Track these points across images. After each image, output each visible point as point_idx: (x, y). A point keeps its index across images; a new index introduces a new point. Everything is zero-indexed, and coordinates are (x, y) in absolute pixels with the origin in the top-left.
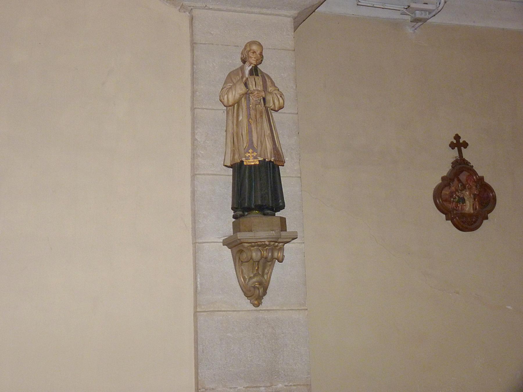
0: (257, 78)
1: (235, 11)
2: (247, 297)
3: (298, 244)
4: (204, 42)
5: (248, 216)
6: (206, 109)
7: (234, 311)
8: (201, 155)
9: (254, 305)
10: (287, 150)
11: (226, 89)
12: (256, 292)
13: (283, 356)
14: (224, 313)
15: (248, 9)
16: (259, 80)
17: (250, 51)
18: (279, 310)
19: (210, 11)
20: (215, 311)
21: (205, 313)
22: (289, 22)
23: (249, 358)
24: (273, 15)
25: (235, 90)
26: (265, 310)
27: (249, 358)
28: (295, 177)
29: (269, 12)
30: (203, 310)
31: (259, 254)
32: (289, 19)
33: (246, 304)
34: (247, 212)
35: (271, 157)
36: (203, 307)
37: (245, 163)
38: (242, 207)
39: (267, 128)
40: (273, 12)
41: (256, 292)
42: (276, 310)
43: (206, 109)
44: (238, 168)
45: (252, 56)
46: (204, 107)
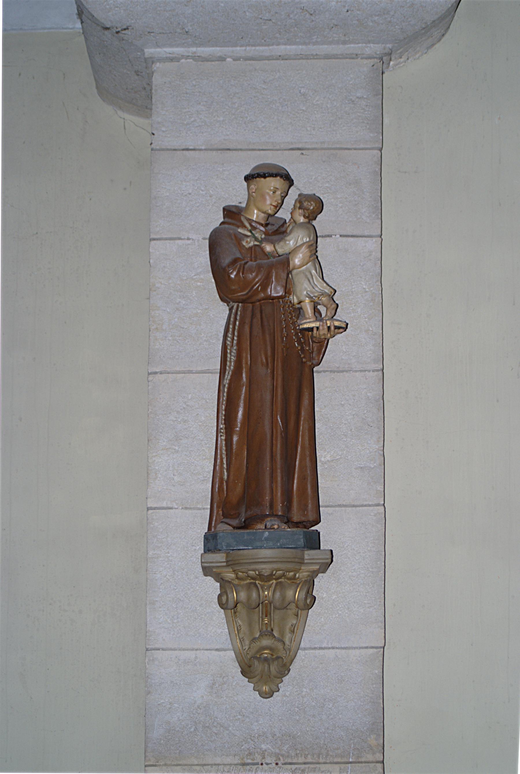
31: (254, 595)
33: (245, 691)
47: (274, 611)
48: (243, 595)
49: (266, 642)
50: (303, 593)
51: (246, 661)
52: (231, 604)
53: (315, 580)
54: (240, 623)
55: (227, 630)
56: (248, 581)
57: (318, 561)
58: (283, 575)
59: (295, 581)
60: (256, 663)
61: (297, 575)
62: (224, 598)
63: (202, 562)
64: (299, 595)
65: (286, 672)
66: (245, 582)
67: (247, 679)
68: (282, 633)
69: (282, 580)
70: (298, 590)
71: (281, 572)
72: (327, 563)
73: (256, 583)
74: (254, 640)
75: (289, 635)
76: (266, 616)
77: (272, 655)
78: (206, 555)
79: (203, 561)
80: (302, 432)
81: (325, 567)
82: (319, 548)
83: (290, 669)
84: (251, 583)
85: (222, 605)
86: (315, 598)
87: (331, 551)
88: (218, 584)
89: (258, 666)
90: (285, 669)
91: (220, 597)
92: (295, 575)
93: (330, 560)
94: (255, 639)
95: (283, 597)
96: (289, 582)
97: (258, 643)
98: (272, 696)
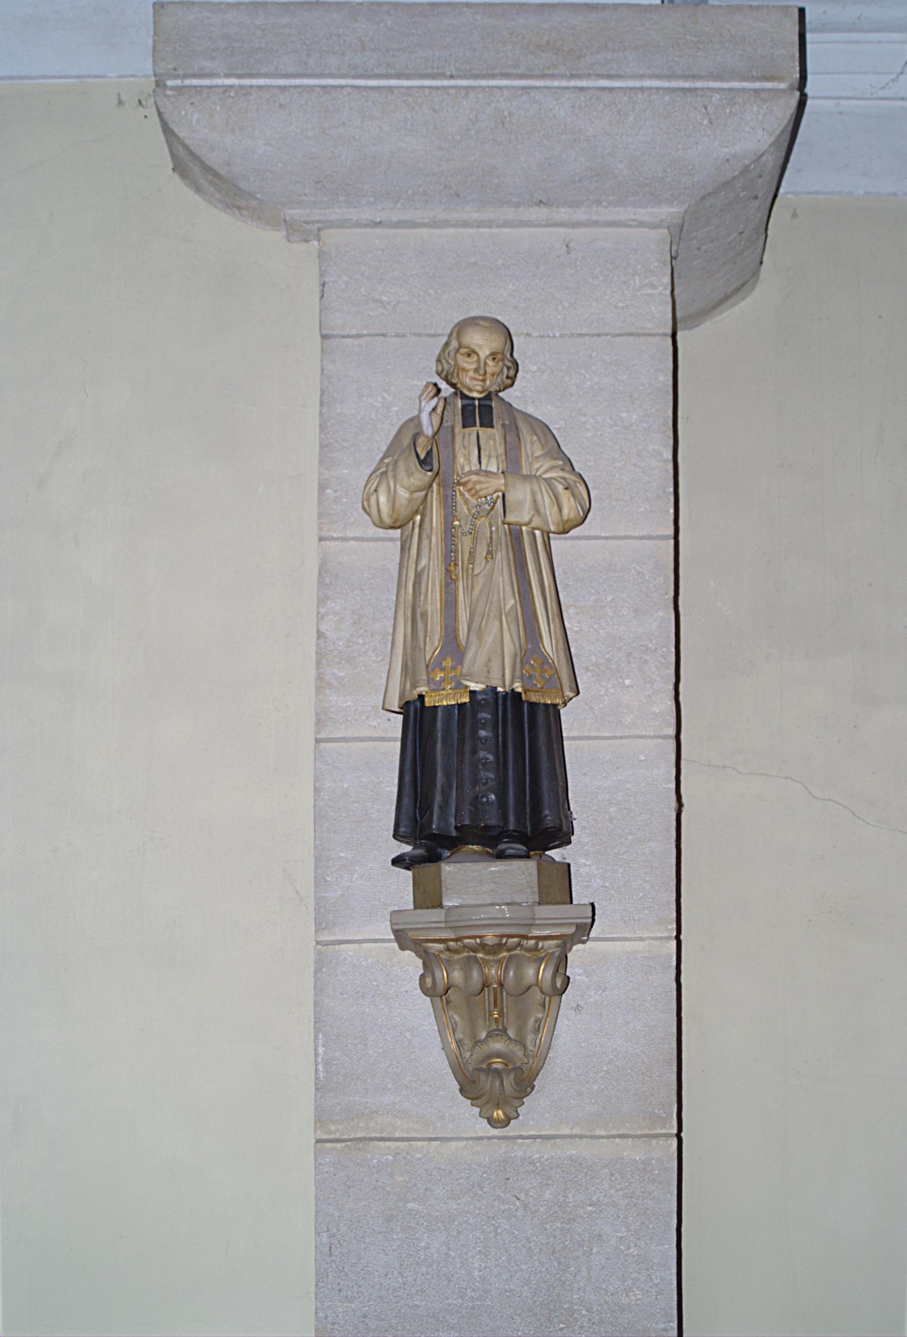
0: (484, 432)
1: (465, 224)
2: (472, 1099)
3: (656, 943)
4: (354, 332)
5: (451, 859)
6: (356, 539)
7: (431, 1139)
8: (335, 683)
9: (492, 1122)
10: (629, 654)
11: (383, 472)
12: (497, 1082)
13: (589, 1269)
14: (399, 1144)
15: (508, 213)
16: (492, 437)
17: (457, 351)
18: (581, 1137)
19: (379, 231)
20: (371, 1139)
21: (339, 1146)
22: (652, 244)
23: (476, 1273)
24: (596, 224)
25: (395, 477)
26: (534, 1137)
27: (476, 1273)
28: (655, 737)
29: (580, 215)
30: (332, 1137)
31: (475, 974)
32: (655, 234)
33: (467, 1117)
34: (449, 849)
35: (512, 683)
36: (333, 1128)
37: (428, 702)
38: (428, 834)
39: (508, 589)
40: (595, 218)
41: (497, 1082)
42: (571, 1137)
43: (356, 539)
44: (417, 717)
45: (466, 366)
46: (349, 534)
47: (507, 998)
48: (457, 975)
49: (498, 1045)
50: (549, 973)
51: (468, 1075)
52: (440, 988)
53: (569, 955)
54: (457, 1018)
55: (436, 1028)
56: (465, 954)
57: (572, 921)
58: (519, 944)
59: (537, 953)
60: (483, 1077)
61: (540, 945)
62: (429, 980)
63: (392, 924)
64: (545, 972)
65: (529, 1089)
66: (462, 956)
67: (470, 1101)
68: (520, 1030)
69: (517, 952)
70: (542, 967)
71: (515, 940)
72: (586, 924)
73: (476, 957)
74: (477, 1042)
75: (532, 1036)
76: (495, 1005)
77: (506, 1065)
78: (416, 413)
79: (394, 921)
80: (524, 802)
81: (583, 931)
82: (571, 903)
83: (534, 1086)
84: (469, 958)
85: (425, 991)
86: (569, 978)
87: (593, 905)
88: (421, 961)
89: (487, 1083)
90: (525, 1084)
91: (422, 977)
92: (537, 944)
93: (590, 920)
94: (479, 1041)
95: (519, 977)
96: (527, 955)
97: (485, 1047)
98: (508, 1125)
